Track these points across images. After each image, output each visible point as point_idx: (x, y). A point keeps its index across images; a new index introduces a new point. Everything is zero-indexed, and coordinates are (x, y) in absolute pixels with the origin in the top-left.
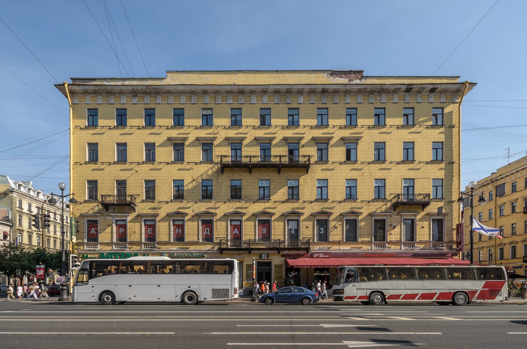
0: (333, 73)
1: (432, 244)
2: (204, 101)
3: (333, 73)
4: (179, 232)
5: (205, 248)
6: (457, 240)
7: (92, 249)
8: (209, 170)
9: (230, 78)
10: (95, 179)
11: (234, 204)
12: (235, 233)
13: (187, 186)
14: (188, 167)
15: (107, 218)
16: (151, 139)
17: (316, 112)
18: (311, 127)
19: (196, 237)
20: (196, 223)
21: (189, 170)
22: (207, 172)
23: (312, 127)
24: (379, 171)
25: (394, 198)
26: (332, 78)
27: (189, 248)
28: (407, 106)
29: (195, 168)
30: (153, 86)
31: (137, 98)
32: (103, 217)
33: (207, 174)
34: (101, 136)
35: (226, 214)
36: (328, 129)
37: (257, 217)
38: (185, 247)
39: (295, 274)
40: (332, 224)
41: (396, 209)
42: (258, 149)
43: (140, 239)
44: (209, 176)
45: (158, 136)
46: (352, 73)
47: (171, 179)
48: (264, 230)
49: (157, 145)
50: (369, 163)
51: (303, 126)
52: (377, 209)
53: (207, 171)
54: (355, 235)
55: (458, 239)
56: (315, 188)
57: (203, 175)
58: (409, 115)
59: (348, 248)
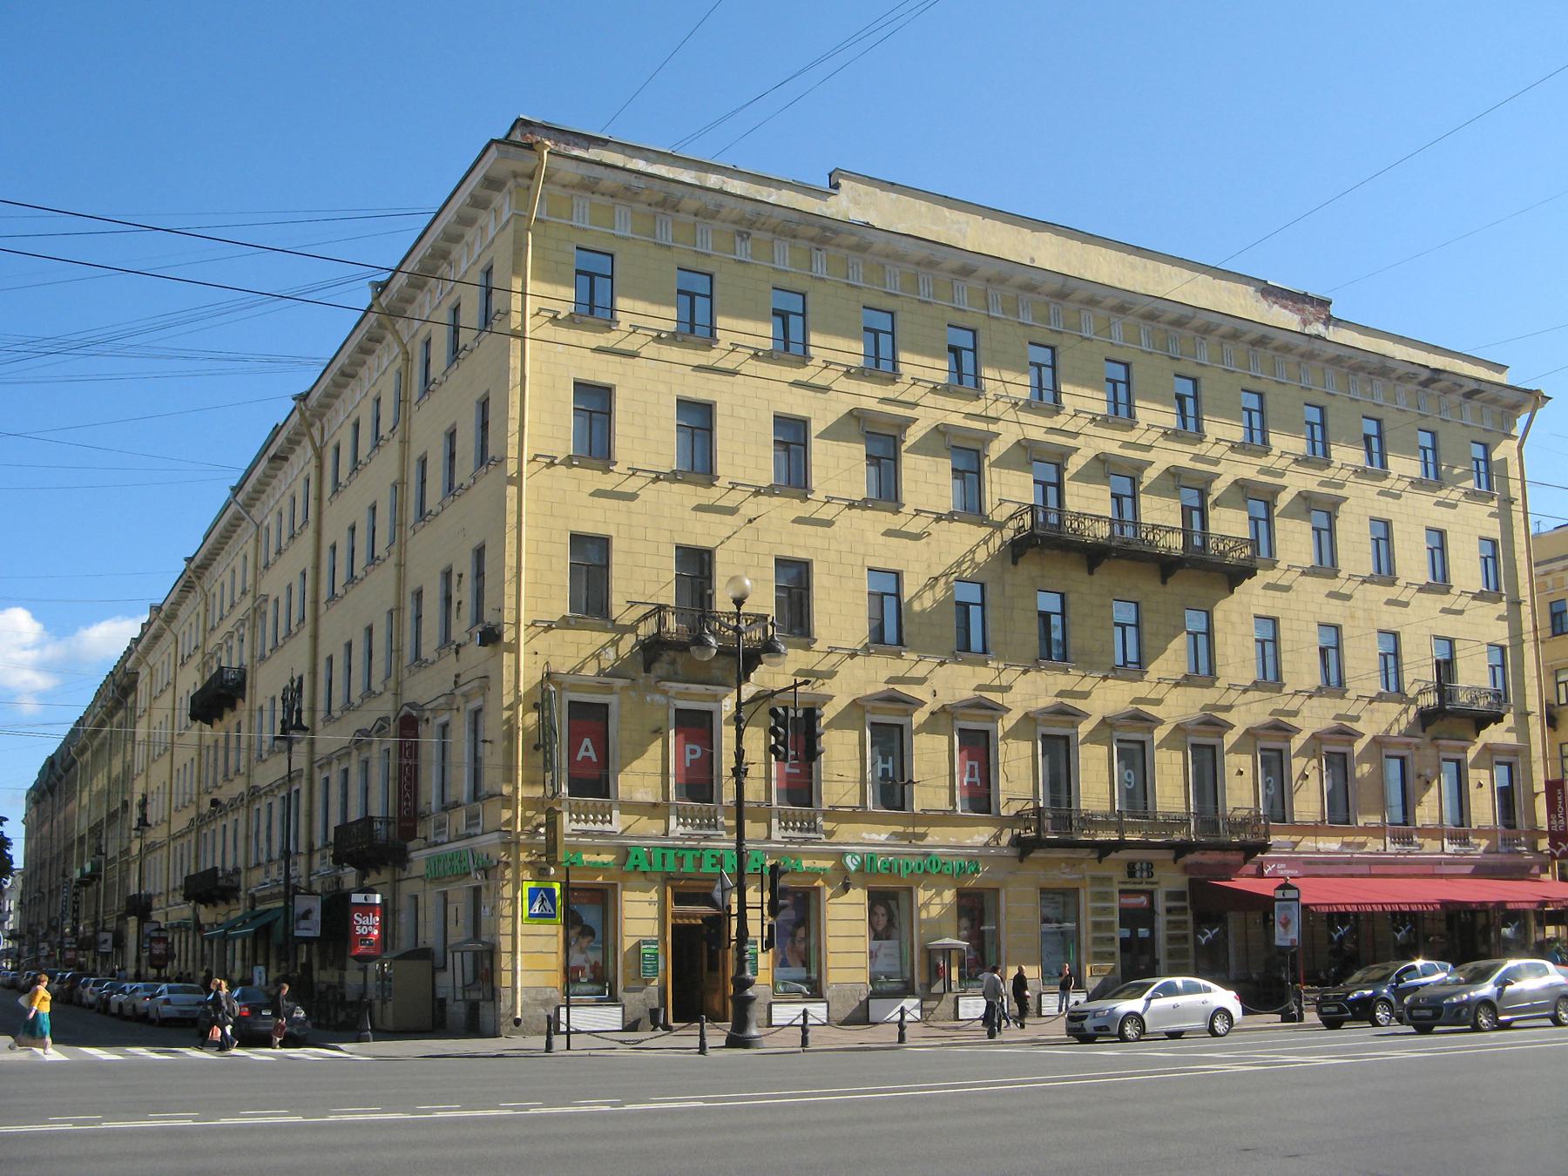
0: (1270, 292)
1: (1499, 835)
2: (699, 243)
3: (1270, 292)
4: (887, 769)
5: (971, 837)
6: (1550, 826)
7: (582, 826)
8: (978, 545)
9: (1019, 237)
10: (601, 530)
11: (1051, 679)
12: (583, 757)
13: (918, 596)
14: (915, 526)
15: (648, 698)
16: (797, 404)
17: (673, 281)
18: (655, 334)
19: (944, 795)
20: (945, 739)
21: (916, 537)
22: (974, 552)
23: (659, 336)
24: (1385, 608)
25: (645, 617)
26: (1264, 304)
27: (924, 836)
28: (958, 319)
29: (934, 534)
30: (825, 221)
31: (749, 243)
32: (632, 694)
33: (972, 560)
34: (623, 360)
35: (1317, 735)
36: (899, 387)
37: (1258, 739)
38: (910, 830)
39: (1214, 932)
40: (1297, 765)
41: (1428, 729)
42: (1176, 506)
43: (763, 794)
44: (980, 569)
45: (819, 395)
46: (1307, 300)
47: (567, 530)
48: (1129, 776)
49: (816, 427)
50: (657, 479)
51: (631, 326)
52: (1391, 725)
53: (972, 551)
54: (809, 781)
55: (1554, 822)
56: (1251, 644)
57: (963, 562)
58: (791, 316)
59: (883, 837)
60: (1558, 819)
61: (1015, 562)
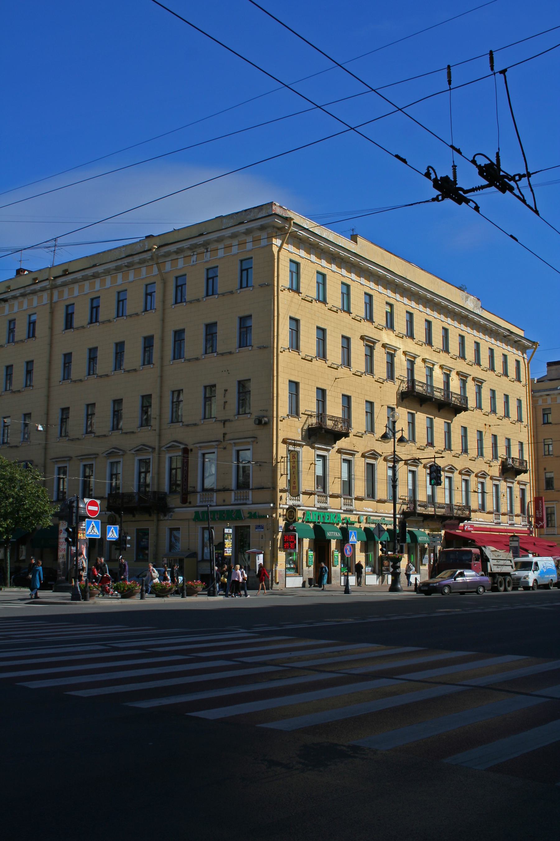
41: (505, 474)
60: (539, 512)
61: (402, 401)
